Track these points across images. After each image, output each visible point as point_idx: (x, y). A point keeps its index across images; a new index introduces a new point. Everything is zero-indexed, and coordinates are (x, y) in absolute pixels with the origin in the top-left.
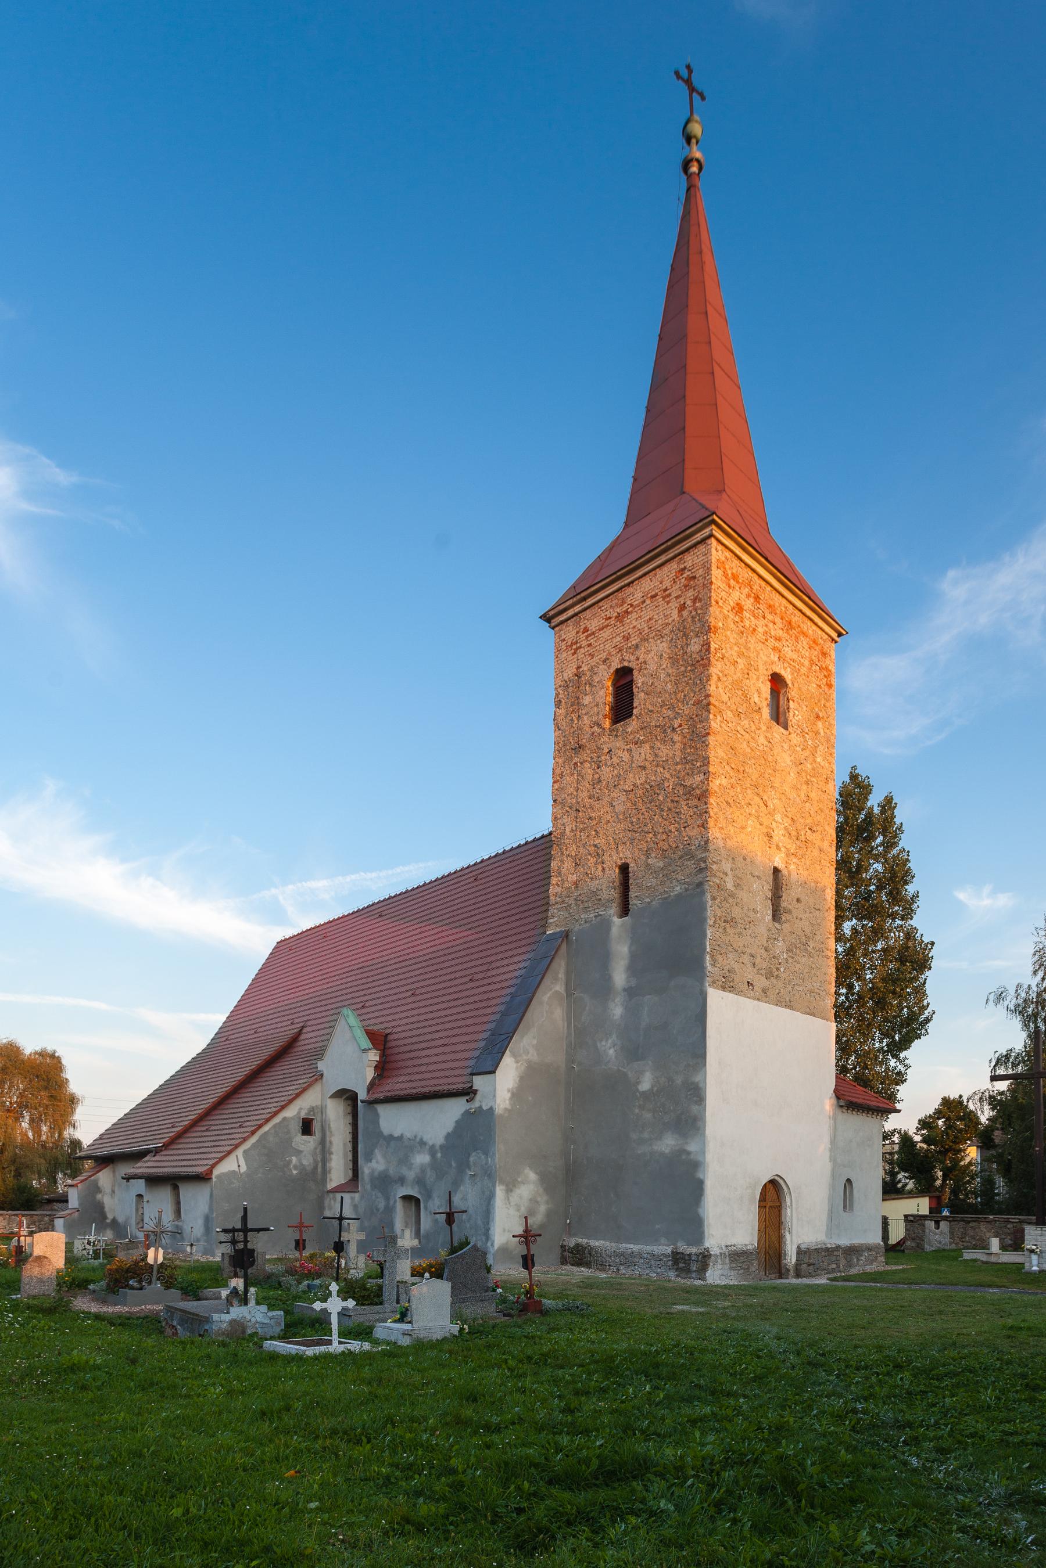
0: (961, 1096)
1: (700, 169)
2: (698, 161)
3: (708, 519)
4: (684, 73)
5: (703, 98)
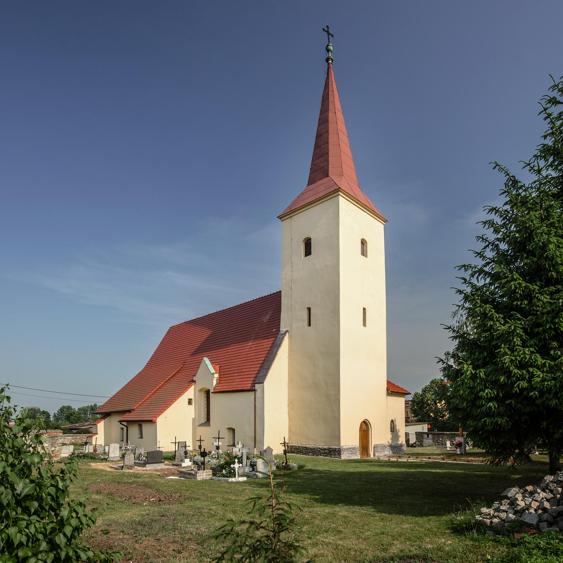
0: (284, 444)
1: (332, 61)
2: (331, 59)
3: (338, 190)
4: (326, 29)
5: (333, 36)
